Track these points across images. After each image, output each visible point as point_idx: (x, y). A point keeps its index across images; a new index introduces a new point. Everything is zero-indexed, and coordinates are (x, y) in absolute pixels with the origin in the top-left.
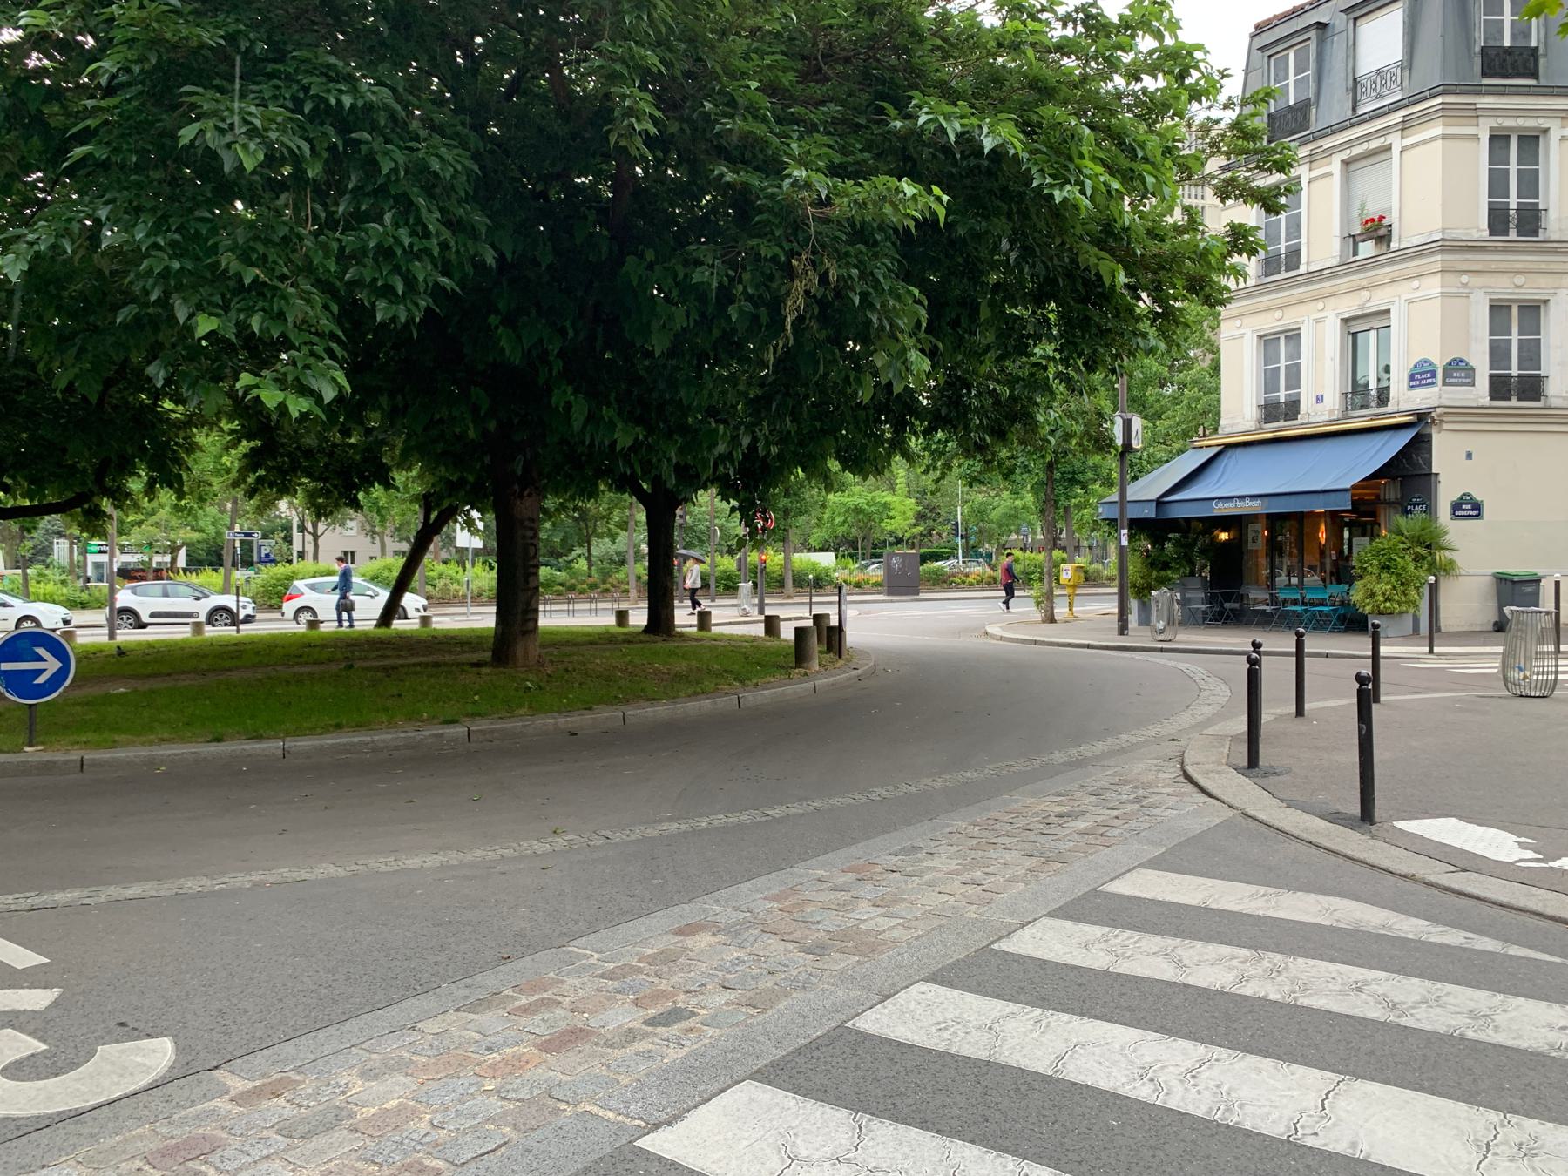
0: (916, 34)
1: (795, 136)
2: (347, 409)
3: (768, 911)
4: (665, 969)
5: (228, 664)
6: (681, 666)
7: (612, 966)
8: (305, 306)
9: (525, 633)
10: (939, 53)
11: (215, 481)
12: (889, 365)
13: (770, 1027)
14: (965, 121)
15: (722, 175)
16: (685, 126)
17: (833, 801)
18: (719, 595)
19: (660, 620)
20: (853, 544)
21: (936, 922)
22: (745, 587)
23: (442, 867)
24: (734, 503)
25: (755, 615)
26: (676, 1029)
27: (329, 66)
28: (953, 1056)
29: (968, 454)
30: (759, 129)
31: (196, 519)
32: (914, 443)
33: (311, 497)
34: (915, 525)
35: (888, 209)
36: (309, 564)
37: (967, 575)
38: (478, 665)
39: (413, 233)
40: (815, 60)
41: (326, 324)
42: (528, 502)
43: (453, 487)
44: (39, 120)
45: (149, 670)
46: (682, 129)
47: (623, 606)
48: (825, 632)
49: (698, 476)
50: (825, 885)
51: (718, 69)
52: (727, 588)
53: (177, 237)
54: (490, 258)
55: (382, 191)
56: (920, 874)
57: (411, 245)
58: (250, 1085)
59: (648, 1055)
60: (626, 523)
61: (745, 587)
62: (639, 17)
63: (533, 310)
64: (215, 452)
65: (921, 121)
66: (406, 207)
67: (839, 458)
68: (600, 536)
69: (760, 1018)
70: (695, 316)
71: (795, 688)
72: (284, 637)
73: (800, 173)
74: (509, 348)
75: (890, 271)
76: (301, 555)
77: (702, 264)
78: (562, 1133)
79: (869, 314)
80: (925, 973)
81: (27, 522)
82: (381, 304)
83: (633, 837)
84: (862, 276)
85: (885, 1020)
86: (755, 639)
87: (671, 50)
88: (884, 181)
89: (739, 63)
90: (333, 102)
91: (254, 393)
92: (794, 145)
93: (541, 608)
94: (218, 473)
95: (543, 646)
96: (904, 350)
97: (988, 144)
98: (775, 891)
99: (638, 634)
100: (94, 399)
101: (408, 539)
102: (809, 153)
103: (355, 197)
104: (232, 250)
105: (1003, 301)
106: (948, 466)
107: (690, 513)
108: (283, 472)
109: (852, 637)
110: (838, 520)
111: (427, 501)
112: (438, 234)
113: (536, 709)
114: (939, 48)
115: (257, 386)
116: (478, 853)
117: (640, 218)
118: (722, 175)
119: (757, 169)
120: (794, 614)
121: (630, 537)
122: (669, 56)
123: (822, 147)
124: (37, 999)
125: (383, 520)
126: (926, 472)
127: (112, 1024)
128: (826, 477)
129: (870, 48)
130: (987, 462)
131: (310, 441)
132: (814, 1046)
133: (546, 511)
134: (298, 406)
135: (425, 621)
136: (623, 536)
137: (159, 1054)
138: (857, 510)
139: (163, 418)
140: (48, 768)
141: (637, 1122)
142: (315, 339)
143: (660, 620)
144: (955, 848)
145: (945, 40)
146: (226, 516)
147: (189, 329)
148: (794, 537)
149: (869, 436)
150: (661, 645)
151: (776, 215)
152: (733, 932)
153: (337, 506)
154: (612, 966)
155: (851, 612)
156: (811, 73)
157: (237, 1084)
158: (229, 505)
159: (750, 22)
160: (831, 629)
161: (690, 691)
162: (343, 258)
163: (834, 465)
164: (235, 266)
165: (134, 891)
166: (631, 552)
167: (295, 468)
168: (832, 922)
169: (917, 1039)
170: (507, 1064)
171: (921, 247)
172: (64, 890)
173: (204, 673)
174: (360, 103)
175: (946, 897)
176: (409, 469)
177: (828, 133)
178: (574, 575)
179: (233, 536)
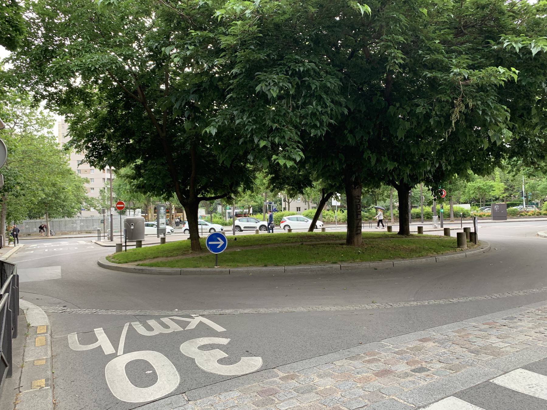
0: (502, 13)
1: (454, 57)
2: (302, 164)
3: (455, 336)
4: (417, 353)
5: (267, 243)
6: (413, 246)
7: (397, 350)
8: (291, 134)
9: (357, 234)
10: (511, 18)
11: (262, 188)
12: (495, 135)
13: (459, 378)
14: (524, 42)
15: (426, 75)
16: (412, 59)
17: (477, 298)
18: (425, 220)
19: (404, 230)
20: (478, 201)
21: (525, 346)
22: (435, 218)
23: (337, 311)
24: (430, 187)
25: (439, 227)
26: (423, 374)
27: (296, 59)
28: (536, 398)
29: (527, 165)
30: (440, 57)
31: (255, 198)
32: (503, 162)
33: (289, 191)
34: (504, 193)
35: (493, 79)
36: (286, 212)
37: (528, 212)
38: (342, 244)
39: (322, 107)
40: (459, 28)
41: (297, 138)
42: (357, 190)
43: (331, 186)
44: (217, 87)
45: (246, 244)
46: (410, 61)
47: (389, 225)
48: (469, 235)
49: (417, 178)
50: (476, 329)
51: (424, 38)
52: (428, 218)
53: (255, 118)
54: (346, 112)
55: (312, 95)
56: (516, 327)
57: (321, 111)
58: (285, 375)
59: (414, 383)
60: (389, 196)
61: (435, 218)
62: (396, 26)
63: (359, 127)
64: (262, 179)
65: (505, 45)
66: (320, 99)
67: (472, 169)
68: (380, 201)
69: (455, 374)
70: (415, 123)
71: (458, 255)
72: (282, 234)
73: (456, 70)
74: (351, 141)
75: (494, 100)
76: (285, 209)
77: (420, 105)
78: (385, 405)
79: (486, 117)
80: (522, 365)
81: (212, 201)
82: (313, 131)
83: (400, 306)
84: (482, 103)
85: (506, 381)
86: (440, 237)
87: (407, 35)
88: (491, 69)
89: (432, 35)
90: (297, 70)
91: (277, 161)
92: (454, 61)
93: (362, 225)
94: (261, 185)
95: (363, 239)
96: (501, 129)
97: (534, 51)
98: (457, 329)
99: (396, 234)
100: (229, 166)
101: (316, 203)
102: (459, 62)
103: (304, 98)
104: (269, 119)
105: (542, 107)
106: (518, 170)
107: (413, 191)
108: (281, 184)
109: (480, 236)
110: (471, 192)
111: (323, 191)
112: (330, 106)
113: (362, 260)
114: (511, 16)
115: (277, 159)
116: (348, 307)
117: (396, 92)
118: (426, 75)
119: (439, 71)
120: (456, 228)
121: (391, 201)
122: (406, 37)
123: (465, 59)
124: (225, 341)
125: (309, 197)
126: (509, 173)
127: (245, 351)
128: (467, 177)
129: (482, 21)
130: (536, 168)
131: (288, 174)
132: (478, 387)
133: (362, 193)
134: (289, 164)
135: (323, 229)
136: (388, 200)
137: (257, 362)
138: (479, 188)
139: (247, 169)
140: (221, 272)
141: (412, 405)
142: (293, 143)
143: (404, 230)
144: (531, 319)
145: (514, 12)
146: (263, 197)
147: (258, 145)
148: (454, 199)
149: (485, 161)
150: (405, 239)
151: (447, 86)
152: (441, 343)
153: (296, 194)
154: (397, 350)
155: (479, 226)
156: (459, 33)
157: (281, 374)
158: (264, 194)
159: (435, 20)
160: (471, 233)
161: (417, 255)
162: (302, 117)
163: (470, 172)
164: (270, 124)
165: (246, 311)
166: (391, 206)
167: (284, 183)
168: (480, 343)
169: (521, 390)
170: (364, 379)
171: (507, 90)
172: (228, 309)
173: (261, 245)
174: (305, 69)
175: (529, 337)
176: (318, 181)
177: (467, 54)
178: (371, 214)
179: (266, 204)
